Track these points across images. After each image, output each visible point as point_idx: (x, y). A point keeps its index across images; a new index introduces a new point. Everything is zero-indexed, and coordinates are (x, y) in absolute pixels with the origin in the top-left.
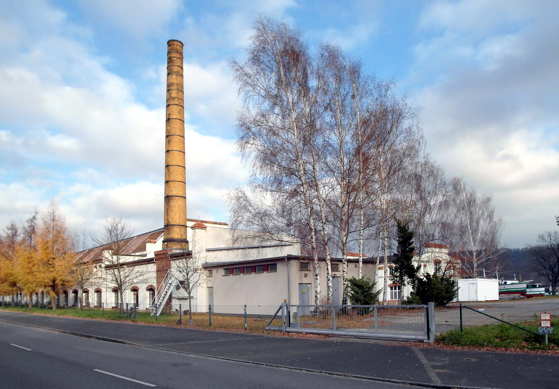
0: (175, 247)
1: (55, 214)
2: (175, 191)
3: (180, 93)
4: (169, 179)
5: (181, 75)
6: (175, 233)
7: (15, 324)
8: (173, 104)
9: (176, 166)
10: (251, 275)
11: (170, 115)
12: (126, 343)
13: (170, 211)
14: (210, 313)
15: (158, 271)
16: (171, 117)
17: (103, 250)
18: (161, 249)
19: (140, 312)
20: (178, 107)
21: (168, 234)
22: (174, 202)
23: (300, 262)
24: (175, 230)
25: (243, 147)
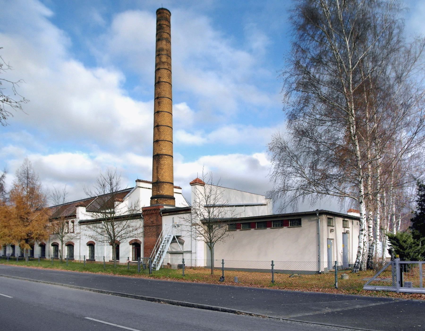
0: (165, 204)
1: (29, 172)
2: (165, 150)
3: (169, 58)
4: (160, 138)
5: (168, 41)
6: (165, 190)
7: (14, 278)
8: (163, 68)
9: (166, 126)
10: (283, 229)
11: (160, 79)
12: (241, 313)
13: (160, 169)
14: (212, 267)
15: (145, 226)
16: (162, 80)
17: (77, 206)
18: (149, 205)
19: (121, 265)
20: (167, 71)
21: (158, 190)
22: (164, 160)
23: (328, 218)
24: (165, 187)
25: (40, 184)
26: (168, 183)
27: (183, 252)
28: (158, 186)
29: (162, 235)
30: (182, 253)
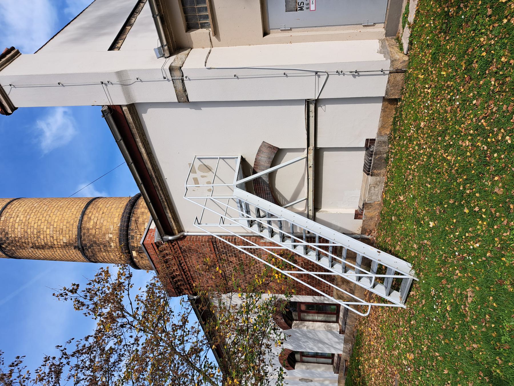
6: (105, 224)
13: (38, 237)
21: (106, 245)
26: (83, 213)
27: (312, 146)
28: (92, 245)
29: (233, 239)
30: (318, 153)
